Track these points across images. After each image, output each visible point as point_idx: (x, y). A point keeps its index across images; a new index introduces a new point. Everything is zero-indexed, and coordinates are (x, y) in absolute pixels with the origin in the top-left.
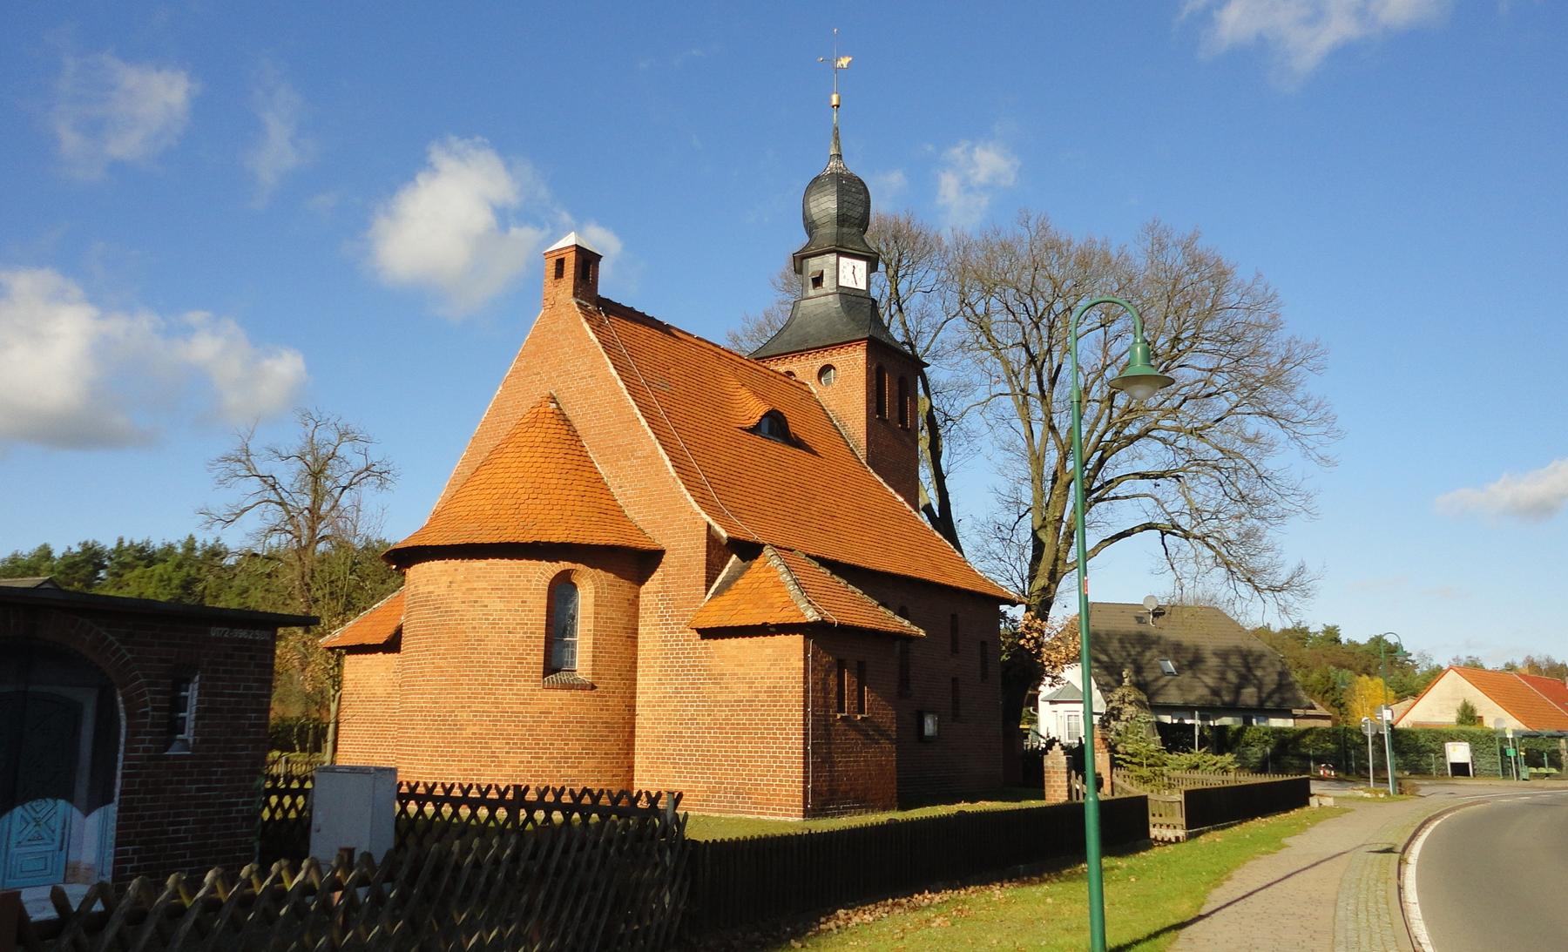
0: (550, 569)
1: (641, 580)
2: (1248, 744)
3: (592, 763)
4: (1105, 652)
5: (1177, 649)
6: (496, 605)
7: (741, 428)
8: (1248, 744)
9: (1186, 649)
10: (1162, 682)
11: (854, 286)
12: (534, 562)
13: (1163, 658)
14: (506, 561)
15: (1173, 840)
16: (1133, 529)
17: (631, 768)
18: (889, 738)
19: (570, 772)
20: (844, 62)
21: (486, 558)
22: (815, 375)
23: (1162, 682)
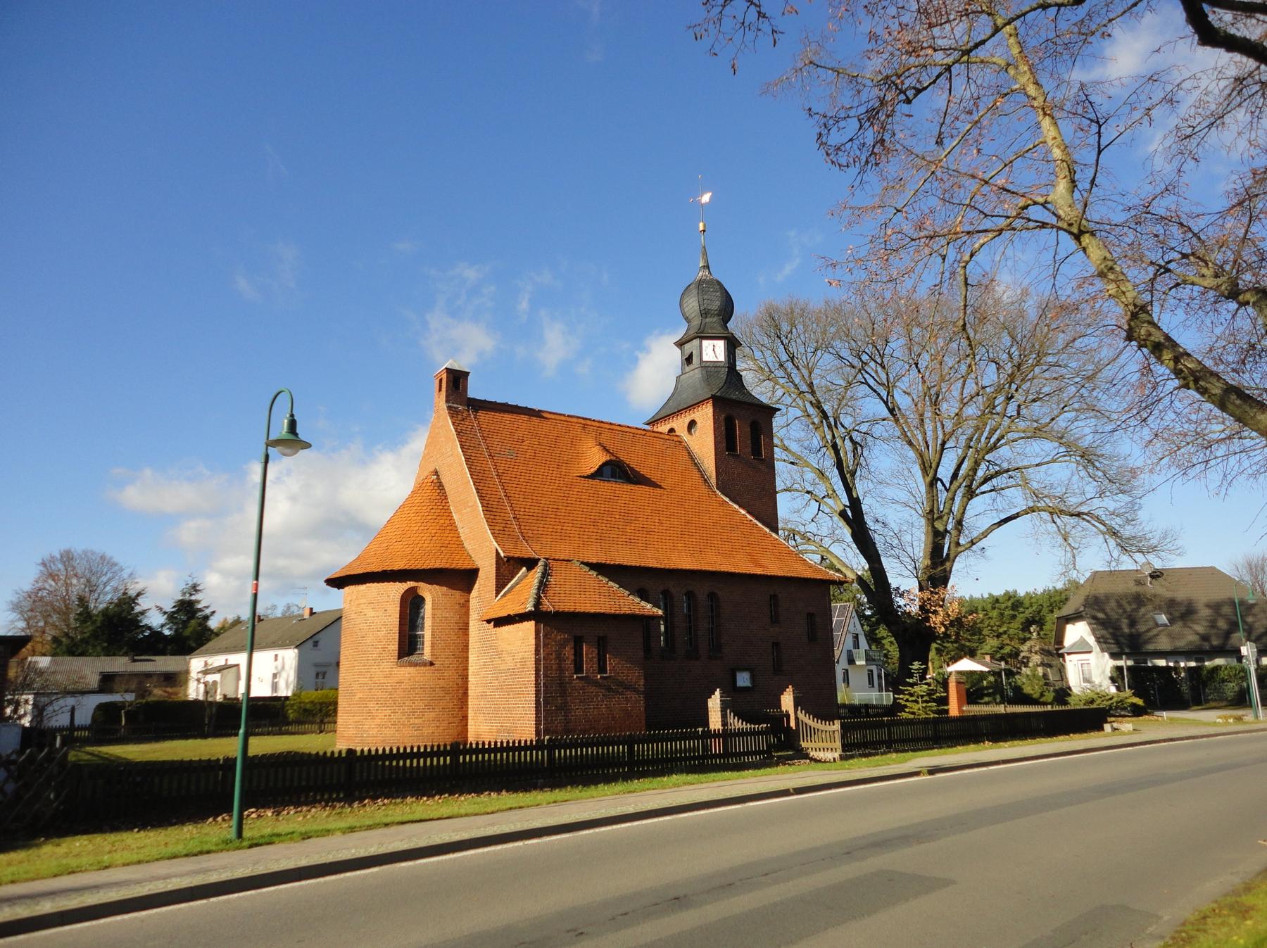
0: (400, 588)
1: (469, 590)
2: (1223, 681)
3: (433, 715)
4: (1103, 611)
5: (1170, 605)
6: (371, 613)
7: (580, 476)
8: (1223, 681)
9: (1179, 604)
10: (1154, 632)
11: (715, 360)
12: (391, 583)
13: (1158, 612)
14: (376, 584)
15: (832, 760)
16: (1018, 513)
17: (465, 717)
18: (636, 690)
19: (416, 721)
20: (706, 198)
21: (365, 583)
22: (686, 429)
23: (1154, 632)
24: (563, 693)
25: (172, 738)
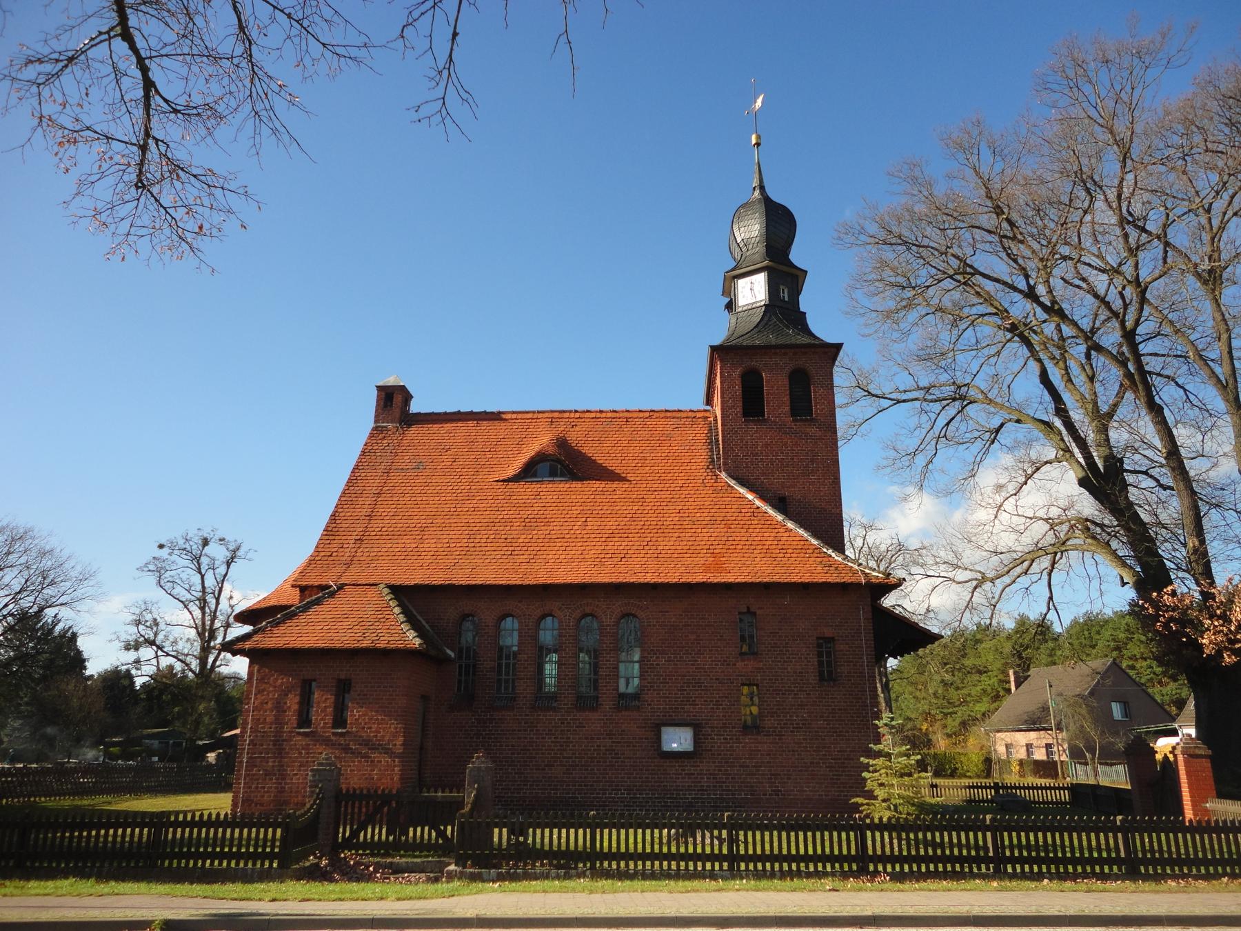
18: (388, 751)
24: (280, 752)
25: (206, 792)
